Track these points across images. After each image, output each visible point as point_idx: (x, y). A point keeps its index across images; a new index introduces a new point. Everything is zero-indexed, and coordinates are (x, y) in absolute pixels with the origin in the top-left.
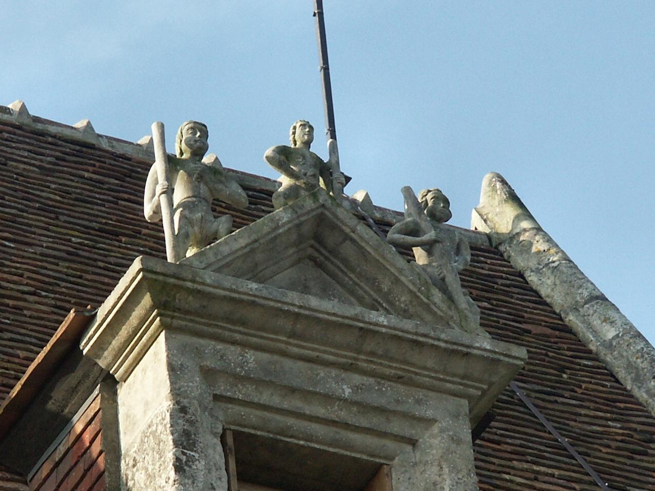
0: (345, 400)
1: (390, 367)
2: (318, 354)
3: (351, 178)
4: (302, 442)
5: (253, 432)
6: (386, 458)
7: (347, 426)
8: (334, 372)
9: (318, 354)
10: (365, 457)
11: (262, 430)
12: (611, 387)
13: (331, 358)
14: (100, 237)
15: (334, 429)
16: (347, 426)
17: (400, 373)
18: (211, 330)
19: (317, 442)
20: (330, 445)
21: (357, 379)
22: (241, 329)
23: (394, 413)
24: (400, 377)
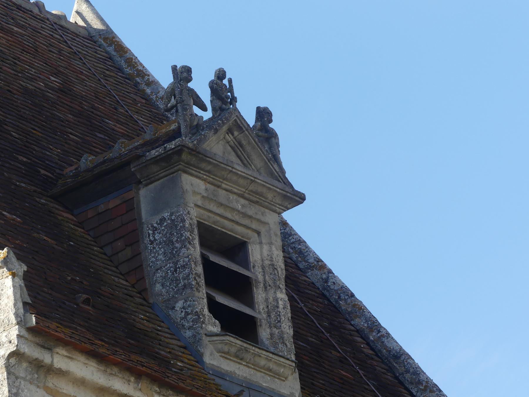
0: (239, 211)
1: (256, 197)
2: (231, 188)
3: (258, 108)
4: (219, 228)
5: (204, 222)
6: (247, 238)
7: (237, 223)
8: (235, 197)
9: (231, 188)
10: (240, 237)
11: (208, 221)
12: (35, 72)
13: (236, 191)
14: (15, 47)
15: (232, 224)
16: (237, 223)
17: (258, 200)
18: (39, 117)
19: (225, 229)
20: (229, 231)
21: (243, 201)
22: (207, 174)
23: (255, 219)
24: (258, 202)
